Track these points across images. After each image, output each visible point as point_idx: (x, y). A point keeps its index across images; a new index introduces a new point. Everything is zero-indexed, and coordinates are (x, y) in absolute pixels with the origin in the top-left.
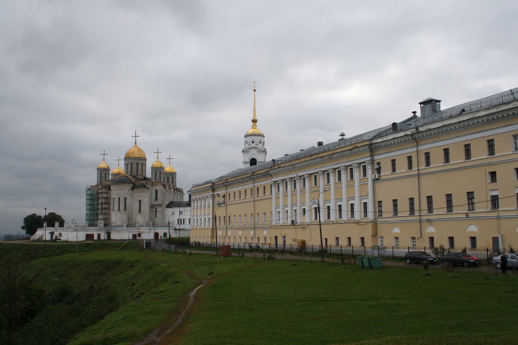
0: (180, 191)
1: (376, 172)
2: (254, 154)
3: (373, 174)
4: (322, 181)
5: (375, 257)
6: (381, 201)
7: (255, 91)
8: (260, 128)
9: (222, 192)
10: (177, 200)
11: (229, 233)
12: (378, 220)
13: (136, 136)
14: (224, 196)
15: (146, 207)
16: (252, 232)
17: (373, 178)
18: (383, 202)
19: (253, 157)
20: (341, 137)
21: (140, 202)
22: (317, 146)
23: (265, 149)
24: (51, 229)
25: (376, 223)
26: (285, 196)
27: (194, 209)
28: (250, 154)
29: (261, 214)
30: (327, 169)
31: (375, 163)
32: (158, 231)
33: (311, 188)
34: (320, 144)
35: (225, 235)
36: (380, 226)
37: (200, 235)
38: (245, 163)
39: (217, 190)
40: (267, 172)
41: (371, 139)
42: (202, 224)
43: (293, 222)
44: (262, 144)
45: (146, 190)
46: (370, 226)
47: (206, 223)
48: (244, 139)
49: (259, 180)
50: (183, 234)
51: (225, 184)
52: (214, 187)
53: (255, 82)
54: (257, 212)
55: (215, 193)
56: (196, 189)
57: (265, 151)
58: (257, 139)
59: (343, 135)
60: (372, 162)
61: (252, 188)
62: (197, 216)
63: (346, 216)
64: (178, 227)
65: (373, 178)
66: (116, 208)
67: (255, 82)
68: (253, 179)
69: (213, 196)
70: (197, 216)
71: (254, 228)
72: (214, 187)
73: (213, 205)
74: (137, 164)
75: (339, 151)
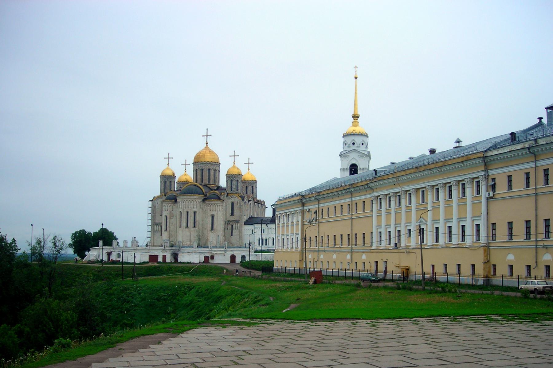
0: (262, 204)
1: (490, 189)
2: (354, 159)
4: (430, 197)
9: (313, 207)
10: (257, 215)
11: (322, 257)
13: (207, 136)
14: (316, 213)
15: (220, 224)
16: (348, 257)
17: (487, 196)
19: (354, 162)
20: (457, 145)
21: (213, 217)
22: (428, 153)
23: (369, 152)
24: (107, 249)
26: (388, 214)
27: (279, 227)
30: (437, 184)
39: (308, 205)
40: (367, 185)
41: (486, 151)
43: (396, 244)
45: (219, 203)
49: (358, 194)
50: (265, 257)
51: (318, 197)
52: (304, 200)
53: (356, 67)
55: (305, 208)
57: (368, 156)
59: (458, 142)
60: (487, 177)
64: (259, 248)
65: (487, 196)
66: (184, 224)
67: (356, 67)
69: (303, 212)
70: (283, 235)
71: (352, 252)
72: (304, 200)
73: (303, 222)
74: (209, 169)
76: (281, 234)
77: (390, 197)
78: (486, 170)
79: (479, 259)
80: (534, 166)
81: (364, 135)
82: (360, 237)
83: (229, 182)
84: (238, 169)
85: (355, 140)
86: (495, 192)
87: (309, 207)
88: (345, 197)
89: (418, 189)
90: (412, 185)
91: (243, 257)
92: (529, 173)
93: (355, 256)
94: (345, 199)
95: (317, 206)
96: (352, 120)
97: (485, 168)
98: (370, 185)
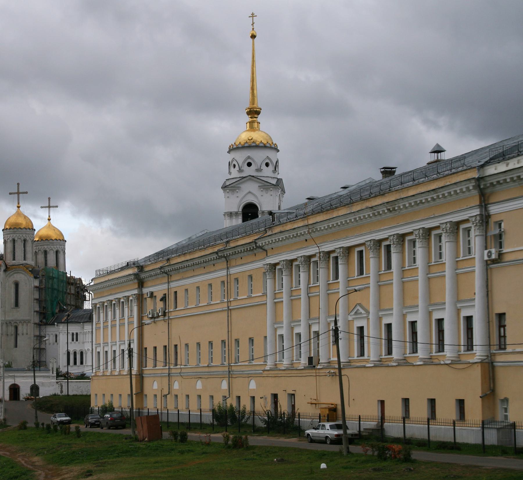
1: (492, 242)
2: (251, 193)
3: (486, 249)
4: (371, 263)
5: (481, 215)
6: (504, 314)
7: (253, 37)
8: (269, 128)
9: (158, 288)
11: (176, 386)
12: (498, 358)
14: (164, 299)
16: (224, 385)
17: (486, 258)
18: (507, 316)
19: (250, 199)
20: (433, 157)
22: (378, 177)
23: (279, 181)
25: (493, 367)
26: (293, 299)
27: (98, 329)
28: (241, 194)
29: (244, 344)
30: (385, 236)
31: (492, 220)
32: (19, 381)
33: (348, 281)
34: (388, 172)
35: (166, 392)
36: (501, 375)
37: (109, 390)
38: (230, 215)
39: (149, 284)
40: (255, 242)
41: (482, 166)
42: (101, 368)
43: (310, 359)
44: (271, 168)
46: (477, 373)
47: (109, 364)
48: (229, 157)
49: (239, 262)
50: (75, 388)
51: (167, 269)
52: (143, 276)
53: (253, 16)
54: (235, 336)
55: (146, 291)
56: (103, 280)
57: (279, 185)
58: (259, 156)
59: (438, 151)
60: (485, 219)
61: (225, 279)
62: (106, 344)
63: (373, 351)
64: (64, 370)
65: (486, 258)
67: (253, 16)
68: (227, 258)
69: (140, 299)
70: (106, 344)
71: (230, 375)
73: (140, 318)
75: (411, 192)
76: (110, 341)
77: (440, 236)
78: (484, 204)
79: (470, 387)
80: (167, 287)
81: (271, 148)
82: (193, 348)
83: (10, 245)
84: (25, 217)
85: (254, 157)
86: (501, 247)
87: (151, 289)
88: (217, 267)
89: (349, 250)
90: (338, 240)
91: (35, 389)
92: (472, 317)
93: (237, 383)
94: (215, 271)
95: (165, 286)
96: (248, 119)
97: (481, 202)
98: (260, 243)
